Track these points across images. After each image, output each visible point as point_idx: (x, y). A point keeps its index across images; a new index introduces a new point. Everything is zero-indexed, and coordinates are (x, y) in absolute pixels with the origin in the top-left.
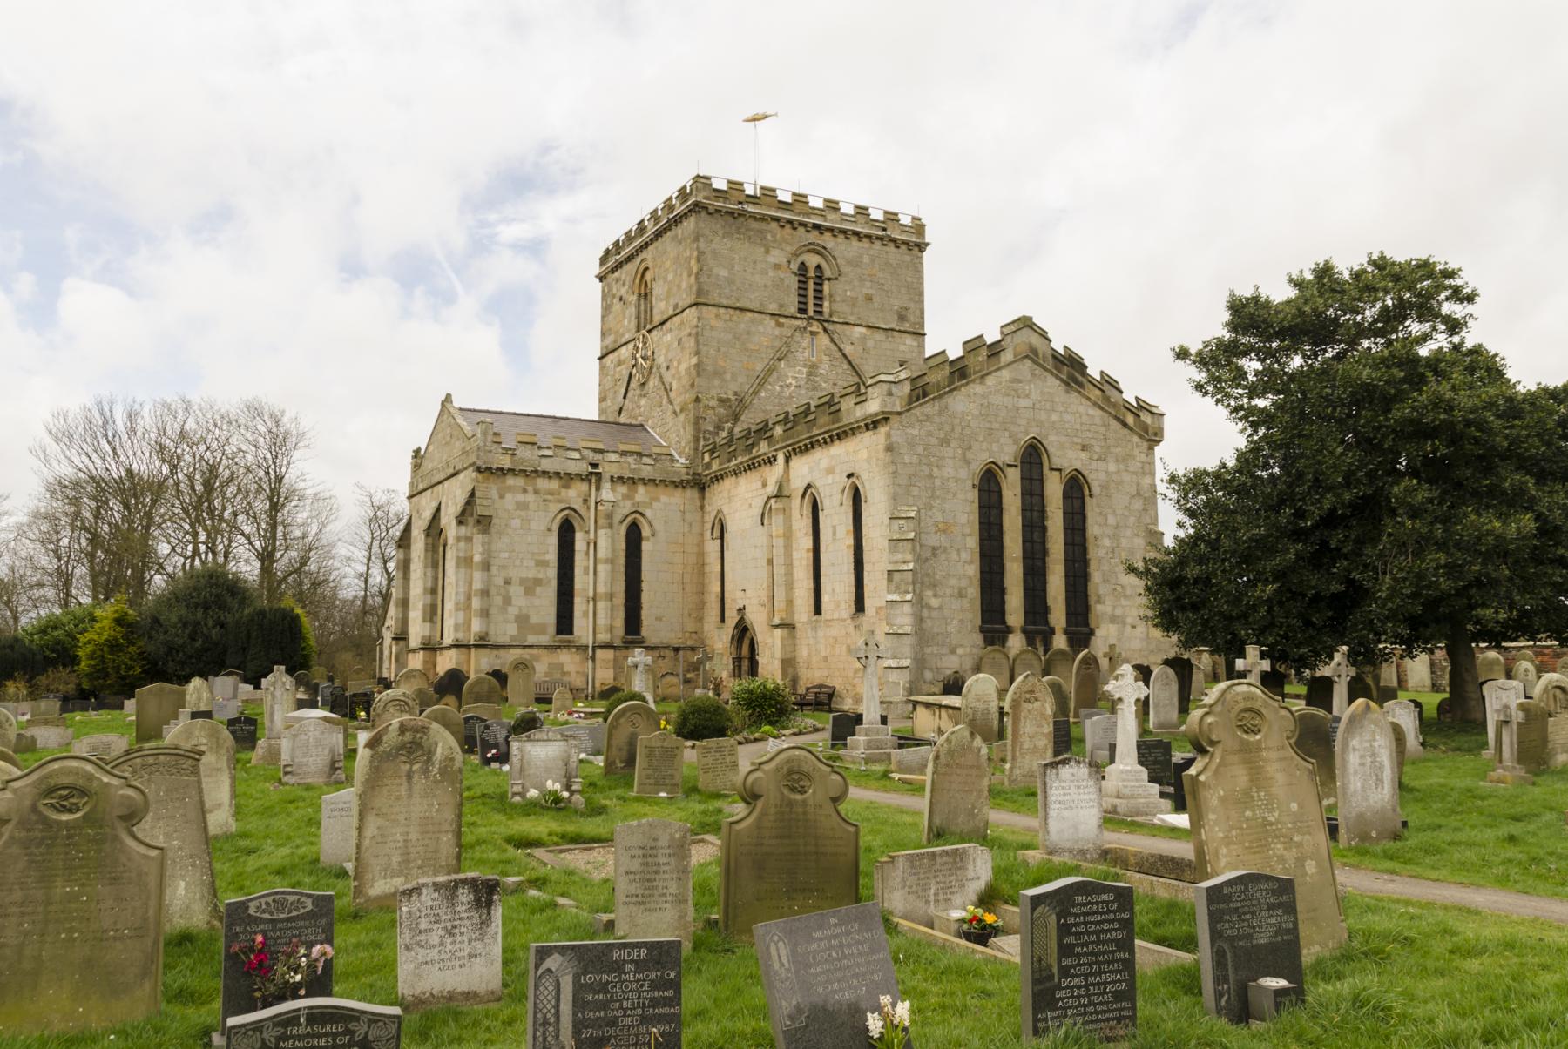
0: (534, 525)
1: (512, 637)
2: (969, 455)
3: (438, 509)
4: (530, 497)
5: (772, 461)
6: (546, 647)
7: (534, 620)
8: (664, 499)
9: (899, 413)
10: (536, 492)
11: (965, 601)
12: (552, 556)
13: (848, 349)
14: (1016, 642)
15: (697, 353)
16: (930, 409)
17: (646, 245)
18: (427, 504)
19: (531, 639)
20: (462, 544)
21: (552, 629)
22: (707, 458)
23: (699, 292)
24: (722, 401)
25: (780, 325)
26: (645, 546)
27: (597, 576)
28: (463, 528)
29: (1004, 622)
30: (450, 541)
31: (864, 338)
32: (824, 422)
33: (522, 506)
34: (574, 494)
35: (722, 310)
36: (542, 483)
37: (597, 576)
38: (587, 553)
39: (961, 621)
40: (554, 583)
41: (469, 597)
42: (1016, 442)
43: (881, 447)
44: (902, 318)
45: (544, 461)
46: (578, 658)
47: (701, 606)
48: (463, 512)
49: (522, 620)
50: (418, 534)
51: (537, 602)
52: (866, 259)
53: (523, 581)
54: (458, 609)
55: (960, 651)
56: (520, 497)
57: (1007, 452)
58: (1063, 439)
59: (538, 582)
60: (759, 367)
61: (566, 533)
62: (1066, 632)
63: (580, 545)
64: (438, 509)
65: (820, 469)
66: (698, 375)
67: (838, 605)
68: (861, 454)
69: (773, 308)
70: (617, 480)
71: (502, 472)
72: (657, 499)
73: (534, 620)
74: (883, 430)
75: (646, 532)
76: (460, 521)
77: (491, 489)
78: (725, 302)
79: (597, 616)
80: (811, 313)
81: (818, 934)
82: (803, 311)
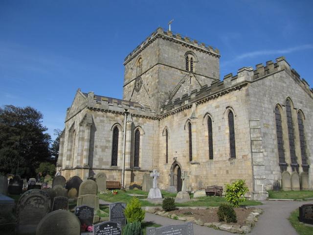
0: (106, 128)
1: (97, 166)
2: (271, 100)
3: (74, 124)
4: (105, 119)
5: (190, 107)
6: (108, 170)
7: (104, 160)
8: (147, 122)
9: (251, 82)
10: (107, 117)
11: (274, 153)
12: (111, 139)
13: (201, 82)
14: (289, 169)
15: (158, 78)
16: (260, 82)
17: (141, 51)
18: (70, 123)
19: (103, 167)
20: (81, 133)
21: (110, 164)
22: (162, 110)
23: (159, 60)
24: (166, 93)
25: (182, 73)
26: (141, 137)
27: (125, 147)
28: (82, 127)
29: (285, 162)
30: (77, 134)
31: (204, 80)
32: (216, 89)
33: (102, 121)
34: (120, 118)
35: (166, 67)
36: (109, 114)
37: (125, 147)
38: (123, 139)
39: (273, 161)
40: (111, 148)
41: (82, 151)
42: (284, 98)
43: (244, 95)
44: (214, 76)
45: (110, 107)
46: (119, 174)
47: (158, 158)
48: (82, 122)
49: (101, 160)
50: (67, 133)
51: (105, 154)
52: (204, 58)
53: (101, 147)
54: (78, 155)
55: (274, 173)
56: (102, 118)
57: (282, 101)
58: (296, 99)
59: (106, 147)
60: (177, 84)
61: (116, 131)
62: (303, 166)
63: (120, 136)
64: (74, 124)
65: (216, 107)
66: (159, 85)
67: (221, 156)
68: (233, 99)
69: (180, 68)
70: (133, 115)
71: (95, 109)
72: (145, 122)
73: (104, 160)
74: (244, 88)
75: (141, 133)
76: (81, 125)
77: (93, 113)
78: (166, 64)
79: (124, 160)
80: (190, 70)
81: (105, 228)
82: (187, 69)
